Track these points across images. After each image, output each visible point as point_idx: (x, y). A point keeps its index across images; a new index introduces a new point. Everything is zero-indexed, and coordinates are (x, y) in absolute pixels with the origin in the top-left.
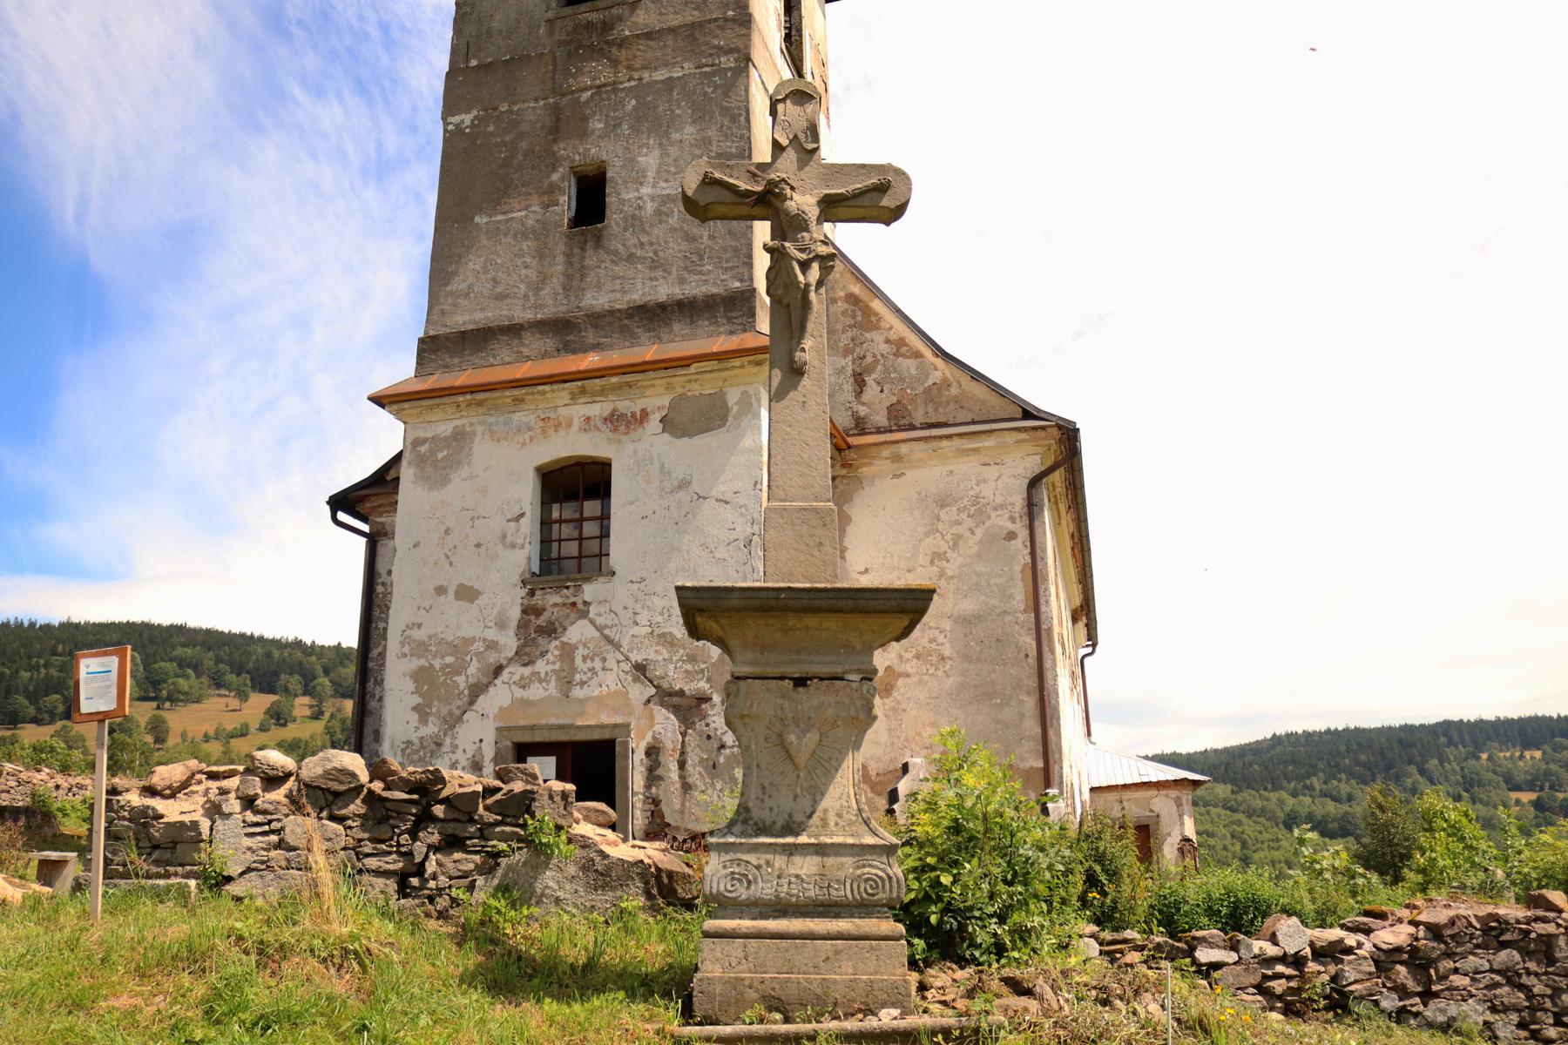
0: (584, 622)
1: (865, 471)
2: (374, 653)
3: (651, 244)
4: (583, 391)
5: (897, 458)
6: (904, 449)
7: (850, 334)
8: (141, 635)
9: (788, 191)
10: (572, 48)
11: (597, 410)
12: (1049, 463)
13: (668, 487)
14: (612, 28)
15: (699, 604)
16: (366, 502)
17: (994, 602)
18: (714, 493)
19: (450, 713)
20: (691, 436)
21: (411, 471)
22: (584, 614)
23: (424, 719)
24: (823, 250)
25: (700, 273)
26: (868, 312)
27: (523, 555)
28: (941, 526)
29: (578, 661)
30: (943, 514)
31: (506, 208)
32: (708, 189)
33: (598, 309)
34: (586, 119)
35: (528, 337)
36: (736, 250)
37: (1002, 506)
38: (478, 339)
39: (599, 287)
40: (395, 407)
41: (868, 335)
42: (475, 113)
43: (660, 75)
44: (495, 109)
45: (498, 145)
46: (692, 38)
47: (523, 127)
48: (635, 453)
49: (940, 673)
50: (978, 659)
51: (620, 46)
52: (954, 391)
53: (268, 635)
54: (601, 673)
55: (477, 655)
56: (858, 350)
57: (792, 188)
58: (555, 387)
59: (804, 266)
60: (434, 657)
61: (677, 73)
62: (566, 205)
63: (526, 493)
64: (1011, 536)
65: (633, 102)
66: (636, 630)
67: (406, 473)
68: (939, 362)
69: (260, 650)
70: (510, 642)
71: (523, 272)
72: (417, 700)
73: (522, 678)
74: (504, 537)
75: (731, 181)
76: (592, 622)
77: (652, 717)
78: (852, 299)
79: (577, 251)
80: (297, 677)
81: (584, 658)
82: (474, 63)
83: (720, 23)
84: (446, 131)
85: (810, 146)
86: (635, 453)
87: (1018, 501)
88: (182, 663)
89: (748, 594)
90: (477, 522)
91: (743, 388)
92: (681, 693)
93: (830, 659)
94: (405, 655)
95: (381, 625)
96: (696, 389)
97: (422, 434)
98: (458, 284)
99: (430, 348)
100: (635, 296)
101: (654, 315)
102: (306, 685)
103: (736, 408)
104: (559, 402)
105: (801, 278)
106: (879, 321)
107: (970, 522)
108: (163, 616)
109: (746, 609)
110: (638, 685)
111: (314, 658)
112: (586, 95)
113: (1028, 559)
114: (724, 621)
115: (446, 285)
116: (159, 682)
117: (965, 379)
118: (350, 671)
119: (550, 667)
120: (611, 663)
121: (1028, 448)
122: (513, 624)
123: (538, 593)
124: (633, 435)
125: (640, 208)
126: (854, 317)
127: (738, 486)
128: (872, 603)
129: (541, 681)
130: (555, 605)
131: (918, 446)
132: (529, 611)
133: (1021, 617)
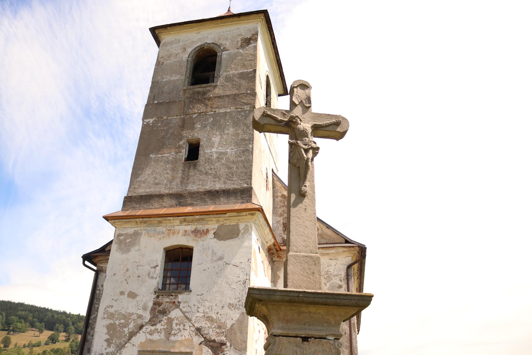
0: (178, 310)
2: (92, 317)
3: (214, 169)
4: (185, 220)
7: (282, 209)
8: (6, 306)
9: (299, 121)
10: (191, 99)
11: (190, 228)
12: (354, 260)
13: (215, 259)
14: (206, 94)
15: (260, 297)
16: (96, 258)
18: (232, 262)
19: (120, 343)
20: (225, 240)
21: (116, 246)
22: (178, 307)
23: (109, 345)
24: (313, 145)
25: (232, 180)
27: (156, 282)
29: (174, 325)
31: (162, 152)
32: (265, 118)
33: (193, 191)
34: (194, 124)
35: (165, 199)
36: (246, 173)
38: (146, 199)
39: (194, 183)
40: (113, 221)
42: (154, 119)
43: (222, 111)
44: (162, 118)
45: (161, 130)
46: (235, 99)
47: (171, 125)
48: (203, 245)
51: (209, 100)
53: (54, 309)
54: (182, 331)
55: (133, 320)
57: (301, 120)
58: (174, 218)
59: (306, 151)
60: (116, 320)
61: (228, 110)
62: (184, 153)
63: (159, 258)
65: (212, 119)
66: (198, 314)
67: (114, 247)
69: (50, 314)
70: (147, 316)
71: (166, 176)
72: (107, 337)
73: (151, 331)
74: (149, 274)
75: (275, 116)
76: (181, 310)
77: (202, 350)
79: (187, 169)
80: (62, 325)
81: (176, 324)
82: (156, 102)
83: (245, 95)
84: (143, 124)
85: (308, 105)
86: (203, 245)
87: (343, 273)
88: (20, 317)
89: (284, 294)
90: (139, 267)
91: (246, 223)
92: (214, 341)
93: (319, 328)
94: (105, 318)
95: (96, 306)
96: (228, 223)
97: (122, 232)
98: (141, 178)
99: (128, 201)
100: (207, 187)
101: (214, 195)
102: (65, 329)
103: (242, 231)
104: (175, 224)
105: (305, 155)
108: (16, 299)
109: (283, 301)
110: (197, 337)
111: (69, 319)
112: (195, 116)
114: (270, 307)
115: (137, 178)
116: (10, 324)
117: (324, 228)
118: (82, 324)
119: (162, 327)
120: (187, 327)
121: (347, 254)
122: (149, 309)
123: (160, 297)
124: (202, 238)
125: (211, 156)
126: (284, 203)
128: (343, 301)
129: (158, 332)
130: (167, 302)
132: (156, 304)
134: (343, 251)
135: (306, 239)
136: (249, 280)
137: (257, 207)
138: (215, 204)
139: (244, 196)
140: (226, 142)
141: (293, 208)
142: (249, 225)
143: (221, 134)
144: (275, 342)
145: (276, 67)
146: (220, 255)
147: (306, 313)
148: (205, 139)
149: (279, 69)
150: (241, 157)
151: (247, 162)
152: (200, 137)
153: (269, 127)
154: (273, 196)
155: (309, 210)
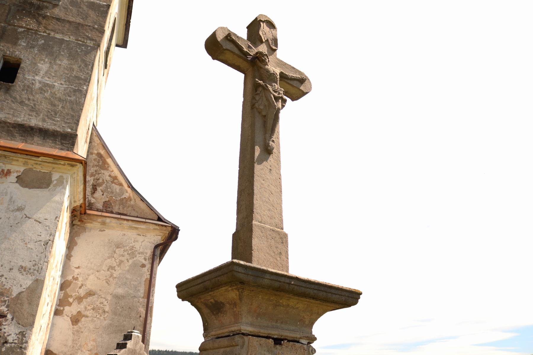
1: (88, 225)
3: (34, 100)
5: (104, 223)
6: (108, 220)
10: (20, 9)
13: (12, 208)
14: (42, 10)
17: (131, 292)
18: (35, 217)
20: (30, 188)
25: (54, 120)
26: (105, 162)
28: (115, 255)
30: (117, 250)
32: (228, 42)
34: (18, 39)
36: (73, 116)
37: (142, 253)
41: (102, 171)
43: (58, 36)
46: (77, 28)
49: (102, 318)
50: (119, 314)
52: (132, 203)
56: (97, 176)
61: (67, 38)
64: (143, 266)
65: (43, 41)
68: (129, 190)
78: (99, 155)
83: (91, 28)
89: (274, 277)
91: (61, 174)
96: (38, 168)
100: (19, 120)
101: (26, 131)
103: (55, 182)
106: (108, 167)
107: (127, 256)
112: (21, 30)
113: (149, 277)
121: (157, 232)
125: (33, 84)
126: (98, 162)
127: (47, 216)
131: (114, 221)
133: (141, 300)
134: (154, 229)
135: (271, 208)
136: (53, 241)
137: (81, 158)
138: (26, 142)
139: (64, 142)
140: (55, 74)
141: (258, 164)
142: (65, 177)
143: (50, 63)
144: (244, 343)
145: (124, 13)
146: (19, 205)
147: (283, 306)
148: (28, 62)
149: (127, 17)
150: (71, 97)
151: (77, 104)
152: (22, 57)
153: (229, 56)
154: (88, 152)
155: (273, 171)
